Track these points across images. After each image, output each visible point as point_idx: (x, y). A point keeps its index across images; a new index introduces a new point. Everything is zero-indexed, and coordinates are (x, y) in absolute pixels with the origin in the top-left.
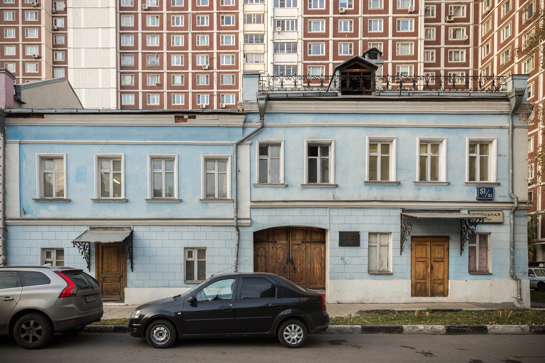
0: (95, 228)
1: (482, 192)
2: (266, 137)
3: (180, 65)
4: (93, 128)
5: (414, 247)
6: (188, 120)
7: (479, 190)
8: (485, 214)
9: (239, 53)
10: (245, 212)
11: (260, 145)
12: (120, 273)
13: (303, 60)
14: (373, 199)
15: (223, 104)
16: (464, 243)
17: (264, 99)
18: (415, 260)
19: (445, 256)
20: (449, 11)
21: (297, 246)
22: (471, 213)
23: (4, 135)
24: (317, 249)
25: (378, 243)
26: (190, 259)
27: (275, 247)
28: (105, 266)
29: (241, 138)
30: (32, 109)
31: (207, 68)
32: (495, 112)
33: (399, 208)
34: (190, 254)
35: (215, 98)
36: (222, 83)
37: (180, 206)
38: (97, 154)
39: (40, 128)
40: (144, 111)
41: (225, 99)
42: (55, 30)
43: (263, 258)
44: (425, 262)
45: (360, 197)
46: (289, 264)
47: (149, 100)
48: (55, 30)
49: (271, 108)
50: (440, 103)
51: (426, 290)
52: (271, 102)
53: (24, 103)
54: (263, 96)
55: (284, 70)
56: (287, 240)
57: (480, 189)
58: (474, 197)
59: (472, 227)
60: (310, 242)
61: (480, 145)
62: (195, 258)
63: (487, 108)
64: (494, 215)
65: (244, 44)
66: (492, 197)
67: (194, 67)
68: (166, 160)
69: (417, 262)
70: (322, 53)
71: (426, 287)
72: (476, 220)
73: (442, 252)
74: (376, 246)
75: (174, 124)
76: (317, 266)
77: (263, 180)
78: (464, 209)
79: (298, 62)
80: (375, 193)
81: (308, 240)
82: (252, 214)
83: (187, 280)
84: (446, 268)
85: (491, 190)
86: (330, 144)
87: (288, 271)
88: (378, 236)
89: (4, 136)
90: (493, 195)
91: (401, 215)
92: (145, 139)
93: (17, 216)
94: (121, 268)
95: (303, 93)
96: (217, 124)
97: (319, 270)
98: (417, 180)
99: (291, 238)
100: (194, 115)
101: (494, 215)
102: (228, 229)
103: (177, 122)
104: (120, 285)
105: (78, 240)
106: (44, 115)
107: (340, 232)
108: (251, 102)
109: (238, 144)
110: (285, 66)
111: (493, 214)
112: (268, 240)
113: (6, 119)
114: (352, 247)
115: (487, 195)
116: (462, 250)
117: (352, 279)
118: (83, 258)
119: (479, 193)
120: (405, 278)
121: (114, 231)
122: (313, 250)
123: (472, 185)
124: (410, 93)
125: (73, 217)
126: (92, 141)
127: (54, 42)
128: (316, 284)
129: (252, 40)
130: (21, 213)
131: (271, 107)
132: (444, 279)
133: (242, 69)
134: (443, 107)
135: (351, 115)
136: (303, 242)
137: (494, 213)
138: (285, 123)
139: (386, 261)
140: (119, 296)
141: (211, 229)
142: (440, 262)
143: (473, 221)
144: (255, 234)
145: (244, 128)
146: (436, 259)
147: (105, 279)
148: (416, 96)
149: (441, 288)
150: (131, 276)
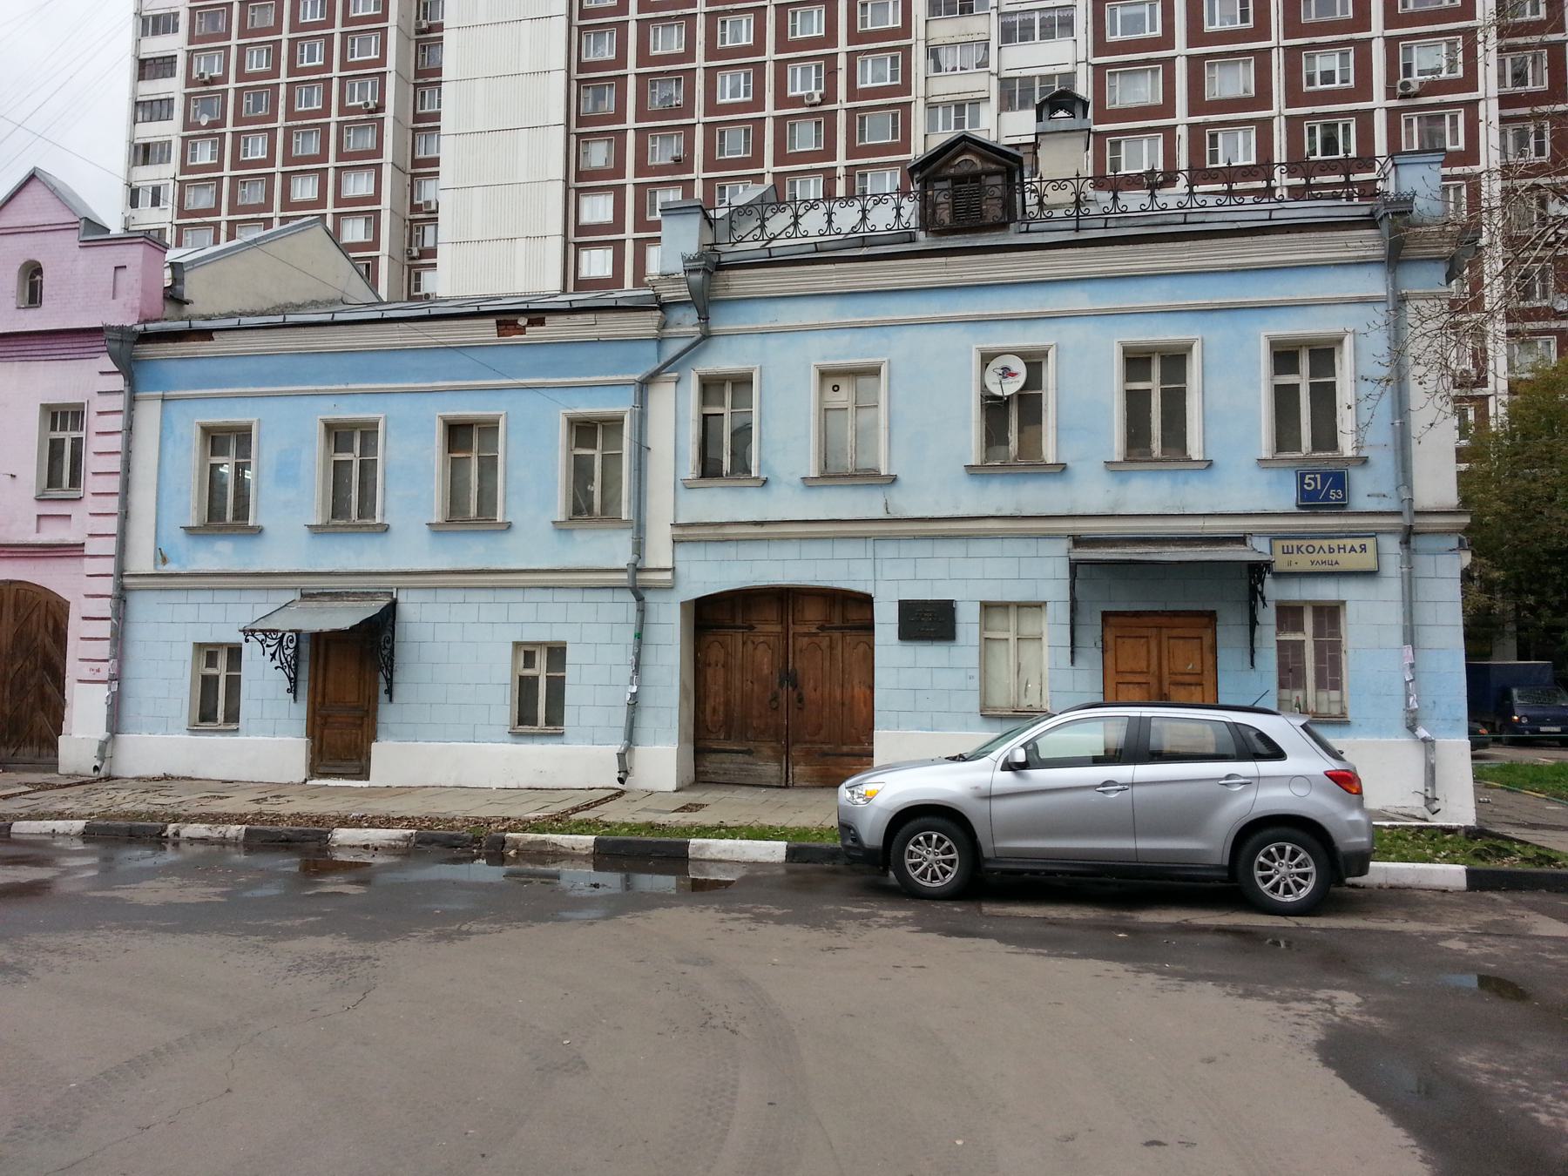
1: (1309, 485)
2: (720, 361)
3: (741, 99)
5: (1111, 642)
8: (1321, 547)
10: (660, 553)
13: (1089, 57)
21: (806, 639)
25: (1012, 632)
26: (528, 672)
27: (749, 642)
28: (330, 687)
29: (656, 366)
31: (817, 99)
34: (529, 660)
37: (508, 541)
42: (423, 32)
43: (721, 672)
46: (785, 688)
48: (423, 32)
49: (727, 287)
50: (1178, 245)
52: (725, 273)
57: (1303, 476)
60: (841, 628)
61: (1312, 353)
62: (540, 670)
63: (1317, 251)
64: (1348, 548)
65: (927, 21)
66: (1343, 499)
67: (782, 100)
70: (1153, 28)
73: (1197, 657)
74: (1007, 639)
75: (497, 341)
77: (709, 469)
78: (1259, 533)
80: (1000, 497)
81: (837, 622)
85: (1338, 480)
88: (1012, 610)
90: (1343, 492)
93: (149, 568)
95: (815, 243)
96: (595, 337)
97: (865, 705)
99: (790, 618)
100: (541, 316)
101: (1347, 550)
105: (257, 626)
106: (215, 335)
108: (676, 276)
110: (1037, 79)
111: (1344, 548)
112: (734, 621)
114: (935, 643)
115: (1328, 491)
118: (276, 668)
123: (1282, 465)
126: (314, 388)
127: (419, 64)
129: (952, 3)
130: (155, 560)
133: (921, 93)
136: (821, 628)
137: (1349, 543)
138: (764, 324)
140: (357, 763)
141: (576, 596)
142: (1190, 684)
145: (660, 341)
146: (1180, 678)
147: (330, 720)
150: (387, 714)
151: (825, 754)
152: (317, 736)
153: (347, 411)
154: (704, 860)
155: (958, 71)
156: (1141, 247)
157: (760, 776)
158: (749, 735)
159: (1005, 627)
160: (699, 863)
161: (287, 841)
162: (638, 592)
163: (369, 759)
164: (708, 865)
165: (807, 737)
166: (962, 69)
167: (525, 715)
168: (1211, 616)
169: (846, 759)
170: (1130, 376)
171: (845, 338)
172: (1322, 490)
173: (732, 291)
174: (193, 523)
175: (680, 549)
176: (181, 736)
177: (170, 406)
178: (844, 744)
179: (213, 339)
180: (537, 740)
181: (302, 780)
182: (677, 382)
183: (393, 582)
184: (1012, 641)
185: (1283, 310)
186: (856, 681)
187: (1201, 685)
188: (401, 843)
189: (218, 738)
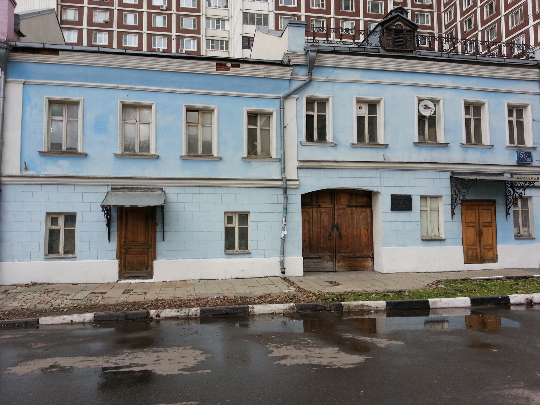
0: (118, 188)
1: (522, 156)
4: (118, 70)
6: (231, 68)
7: (518, 153)
9: (201, 38)
11: (508, 107)
12: (148, 243)
14: (423, 161)
15: (183, 49)
16: (455, 207)
17: (315, 51)
18: (466, 225)
19: (493, 220)
20: (180, 44)
21: (342, 210)
22: (514, 176)
23: (5, 72)
24: (363, 214)
27: (318, 212)
28: (129, 235)
29: (287, 92)
30: (44, 44)
31: (165, 8)
32: (528, 78)
33: (449, 170)
34: (230, 220)
35: (174, 43)
36: (182, 26)
37: (220, 165)
38: (186, 104)
39: (53, 66)
40: (178, 55)
41: (157, 42)
44: (475, 227)
45: (411, 159)
46: (334, 230)
47: (95, 39)
51: (477, 256)
53: (23, 36)
54: (314, 48)
55: (254, 18)
56: (332, 204)
57: (520, 153)
58: (514, 160)
59: (521, 191)
62: (61, 225)
63: (521, 75)
66: (531, 161)
68: (203, 112)
69: (467, 227)
70: (294, 4)
71: (477, 253)
72: (525, 184)
73: (490, 216)
76: (363, 232)
78: (507, 172)
79: (269, 11)
81: (354, 204)
82: (300, 175)
83: (226, 250)
84: (494, 233)
85: (529, 155)
86: (379, 102)
87: (333, 238)
89: (6, 75)
90: (531, 159)
91: (451, 177)
92: (180, 87)
93: (17, 172)
94: (150, 236)
95: (349, 47)
97: (365, 237)
98: (464, 142)
99: (336, 202)
100: (238, 63)
102: (274, 191)
103: (219, 70)
104: (148, 257)
106: (60, 52)
107: (391, 195)
109: (286, 97)
112: (312, 203)
113: (11, 53)
114: (404, 212)
115: (527, 159)
116: (508, 213)
117: (406, 246)
119: (520, 157)
120: (458, 244)
121: (142, 192)
122: (359, 214)
123: (511, 148)
124: (450, 55)
125: (90, 174)
126: (116, 85)
128: (363, 252)
131: (319, 60)
132: (492, 245)
133: (204, 13)
134: (363, 62)
135: (398, 73)
136: (348, 206)
138: (332, 78)
139: (437, 226)
143: (520, 185)
144: (303, 196)
146: (485, 224)
148: (455, 58)
149: (490, 254)
150: (160, 246)
151: (350, 257)
152: (123, 259)
153: (256, 107)
154: (437, 308)
155: (217, 7)
156: (470, 65)
157: (325, 268)
158: (319, 251)
159: (430, 204)
160: (434, 310)
161: (227, 314)
162: (285, 190)
163: (152, 269)
164: (438, 310)
165: (343, 251)
166: (219, 7)
167: (229, 246)
168: (494, 202)
169: (359, 259)
170: (249, 123)
171: (367, 88)
172: (525, 157)
173: (321, 62)
174: (44, 149)
175: (301, 171)
176: (40, 262)
177: (28, 87)
178: (358, 253)
179: (59, 55)
180: (237, 256)
181: (116, 281)
182: (297, 99)
183: (163, 183)
184: (429, 211)
185: (510, 94)
186: (362, 228)
187: (492, 226)
188: (289, 311)
189: (63, 262)
